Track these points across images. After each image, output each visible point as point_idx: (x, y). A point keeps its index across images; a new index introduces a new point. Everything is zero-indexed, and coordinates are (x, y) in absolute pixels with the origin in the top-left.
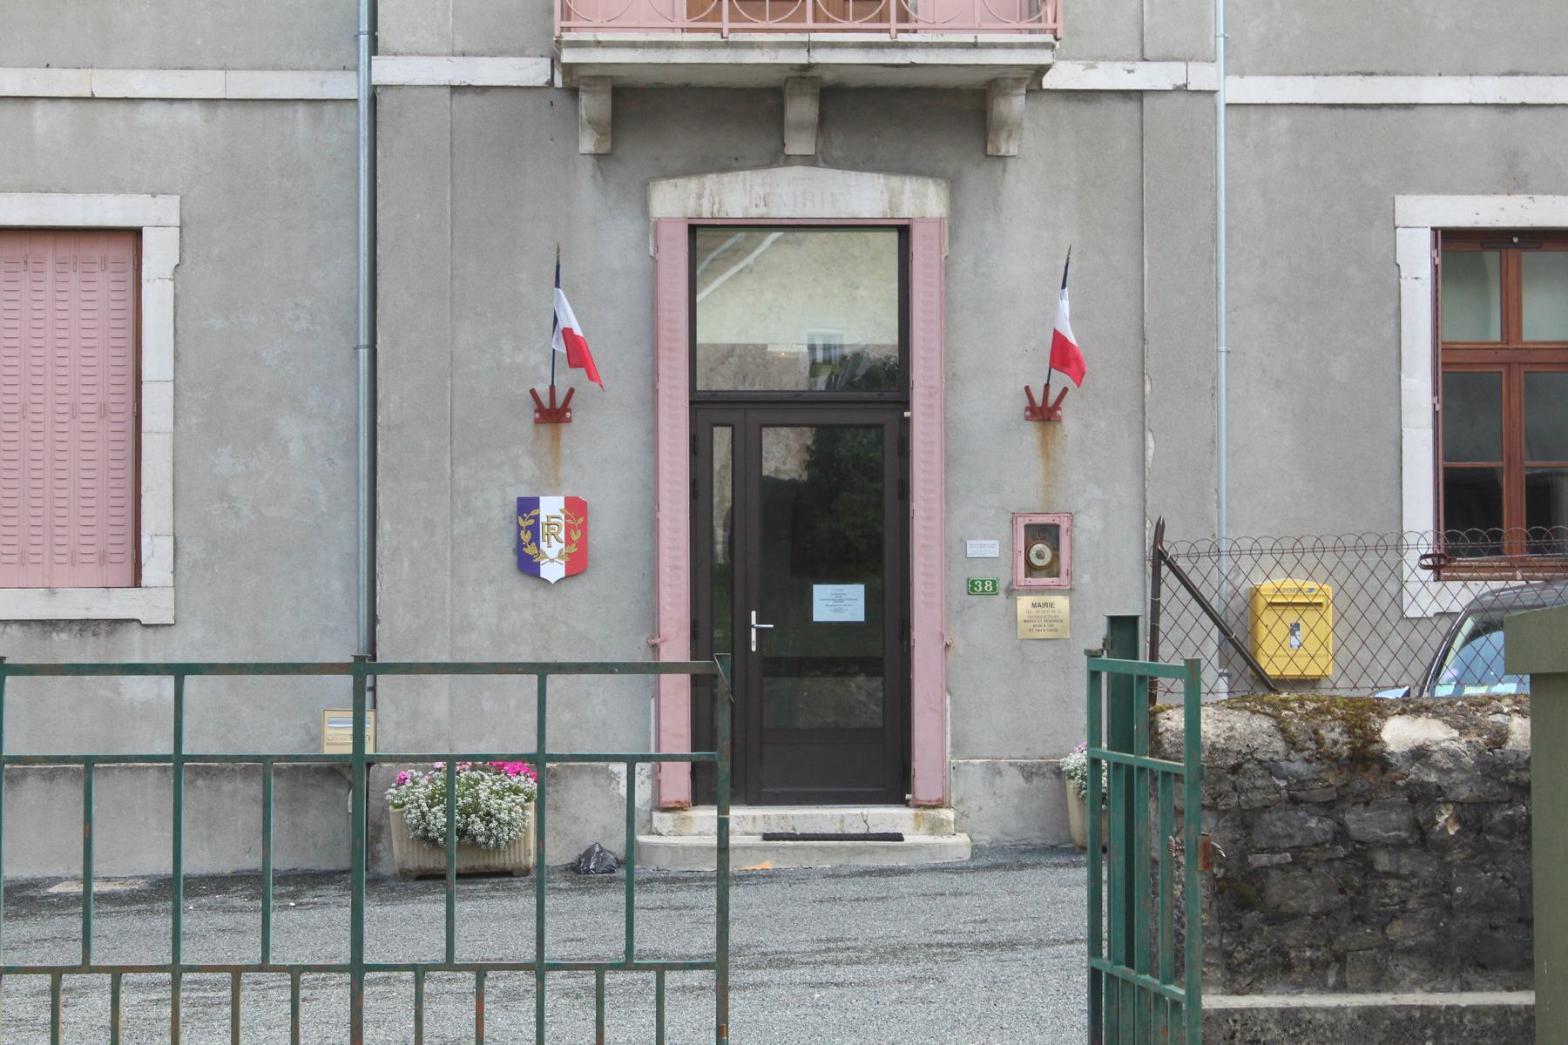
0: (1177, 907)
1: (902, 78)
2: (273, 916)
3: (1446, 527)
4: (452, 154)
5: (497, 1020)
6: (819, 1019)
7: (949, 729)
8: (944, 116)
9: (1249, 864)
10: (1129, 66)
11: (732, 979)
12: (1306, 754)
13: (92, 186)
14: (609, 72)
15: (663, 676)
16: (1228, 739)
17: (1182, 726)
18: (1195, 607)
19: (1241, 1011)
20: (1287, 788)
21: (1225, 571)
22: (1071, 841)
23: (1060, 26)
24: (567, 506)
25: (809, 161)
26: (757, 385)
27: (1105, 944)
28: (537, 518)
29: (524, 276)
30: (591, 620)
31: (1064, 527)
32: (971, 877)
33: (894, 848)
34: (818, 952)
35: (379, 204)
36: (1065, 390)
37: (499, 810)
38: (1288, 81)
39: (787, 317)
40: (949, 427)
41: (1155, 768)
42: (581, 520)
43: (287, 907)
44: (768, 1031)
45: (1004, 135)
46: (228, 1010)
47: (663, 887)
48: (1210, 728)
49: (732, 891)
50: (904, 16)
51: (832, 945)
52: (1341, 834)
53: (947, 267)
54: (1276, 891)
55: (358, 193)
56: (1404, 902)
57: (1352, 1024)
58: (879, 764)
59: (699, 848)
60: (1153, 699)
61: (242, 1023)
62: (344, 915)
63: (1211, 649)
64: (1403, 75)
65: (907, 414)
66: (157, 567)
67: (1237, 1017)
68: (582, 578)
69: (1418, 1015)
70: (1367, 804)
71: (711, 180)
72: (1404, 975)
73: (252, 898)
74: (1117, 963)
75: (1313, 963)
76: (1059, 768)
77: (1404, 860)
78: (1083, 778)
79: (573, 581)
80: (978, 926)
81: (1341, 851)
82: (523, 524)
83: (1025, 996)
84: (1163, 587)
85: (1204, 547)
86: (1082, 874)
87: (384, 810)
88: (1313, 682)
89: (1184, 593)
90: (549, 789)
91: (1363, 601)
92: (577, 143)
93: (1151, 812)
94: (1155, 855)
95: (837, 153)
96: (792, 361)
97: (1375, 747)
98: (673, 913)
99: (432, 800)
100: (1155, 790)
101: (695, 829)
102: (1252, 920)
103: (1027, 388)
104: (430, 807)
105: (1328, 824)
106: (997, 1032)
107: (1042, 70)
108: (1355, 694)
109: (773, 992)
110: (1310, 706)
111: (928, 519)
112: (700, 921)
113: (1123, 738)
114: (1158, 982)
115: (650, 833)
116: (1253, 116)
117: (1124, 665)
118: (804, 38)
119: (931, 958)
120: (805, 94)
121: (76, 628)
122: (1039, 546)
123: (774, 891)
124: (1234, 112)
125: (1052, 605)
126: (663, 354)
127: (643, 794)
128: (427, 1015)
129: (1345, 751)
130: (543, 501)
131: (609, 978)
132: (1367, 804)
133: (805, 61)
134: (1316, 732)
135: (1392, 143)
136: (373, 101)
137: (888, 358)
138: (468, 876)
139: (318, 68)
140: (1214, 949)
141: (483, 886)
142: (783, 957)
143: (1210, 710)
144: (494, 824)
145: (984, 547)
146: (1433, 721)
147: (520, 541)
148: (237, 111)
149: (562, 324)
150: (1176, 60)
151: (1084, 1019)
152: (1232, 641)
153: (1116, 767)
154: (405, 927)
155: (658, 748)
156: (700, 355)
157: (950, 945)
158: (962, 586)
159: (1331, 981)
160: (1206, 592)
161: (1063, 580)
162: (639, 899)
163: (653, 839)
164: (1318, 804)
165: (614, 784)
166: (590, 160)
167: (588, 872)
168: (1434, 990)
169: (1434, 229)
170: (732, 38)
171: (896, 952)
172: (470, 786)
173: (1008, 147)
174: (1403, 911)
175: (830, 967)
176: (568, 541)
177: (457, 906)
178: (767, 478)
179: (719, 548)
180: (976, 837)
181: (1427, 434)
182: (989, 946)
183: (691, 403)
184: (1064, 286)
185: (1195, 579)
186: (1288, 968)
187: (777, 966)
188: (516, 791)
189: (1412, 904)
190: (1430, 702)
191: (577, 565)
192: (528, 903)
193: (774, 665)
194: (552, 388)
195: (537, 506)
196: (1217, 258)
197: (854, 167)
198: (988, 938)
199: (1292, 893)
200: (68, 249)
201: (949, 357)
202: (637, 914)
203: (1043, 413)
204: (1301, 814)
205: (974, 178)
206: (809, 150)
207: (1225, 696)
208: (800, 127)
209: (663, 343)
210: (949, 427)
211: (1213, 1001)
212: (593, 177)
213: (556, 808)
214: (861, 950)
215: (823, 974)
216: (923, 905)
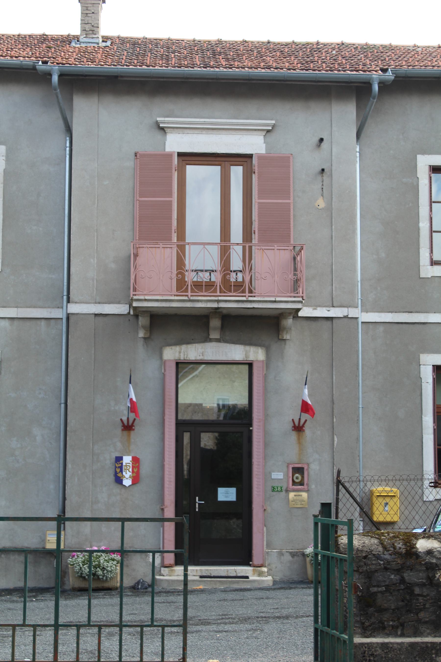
0: (345, 606)
1: (250, 312)
2: (27, 604)
3: (438, 473)
4: (95, 337)
5: (105, 643)
6: (219, 644)
7: (265, 539)
8: (265, 326)
9: (370, 591)
10: (328, 309)
11: (188, 629)
12: (390, 552)
14: (149, 310)
15: (165, 523)
16: (363, 546)
17: (347, 542)
18: (351, 500)
19: (368, 644)
20: (384, 564)
21: (362, 487)
22: (308, 579)
23: (304, 295)
26: (198, 417)
27: (320, 617)
28: (122, 464)
29: (119, 379)
30: (140, 502)
32: (272, 592)
34: (219, 619)
35: (69, 354)
37: (107, 567)
38: (383, 315)
39: (208, 394)
40: (266, 433)
41: (337, 557)
42: (137, 464)
43: (32, 601)
44: (201, 649)
45: (285, 332)
46: (11, 639)
47: (165, 594)
48: (356, 543)
49: (189, 596)
50: (251, 291)
51: (224, 617)
52: (402, 581)
53: (265, 377)
54: (380, 600)
55: (62, 350)
56: (424, 605)
57: (406, 648)
59: (178, 581)
60: (336, 532)
61: (16, 644)
62: (52, 604)
63: (357, 514)
64: (422, 313)
65: (251, 428)
67: (366, 646)
68: (137, 485)
69: (429, 645)
70: (411, 570)
71: (184, 347)
72: (424, 631)
73: (20, 597)
74: (324, 626)
75: (393, 626)
76: (304, 553)
77: (425, 590)
78: (312, 557)
79: (134, 486)
80: (275, 610)
81: (402, 587)
82: (117, 466)
83: (291, 636)
84: (340, 493)
86: (312, 591)
87: (67, 566)
88: (391, 523)
89: (347, 495)
90: (125, 559)
91: (410, 498)
92: (138, 333)
93: (336, 572)
94: (338, 587)
96: (211, 409)
97: (414, 550)
98: (168, 604)
99: (84, 563)
100: (337, 564)
101: (176, 574)
102: (372, 612)
103: (293, 420)
104: (83, 565)
105: (398, 577)
106: (282, 649)
107: (298, 310)
108: (407, 531)
109: (202, 634)
110: (392, 535)
111: (258, 465)
112: (177, 607)
113: (326, 547)
114: (338, 633)
115: (160, 575)
116: (371, 326)
117: (326, 520)
118: (216, 298)
119: (258, 622)
122: (297, 475)
123: (204, 596)
124: (364, 325)
127: (158, 561)
128: (81, 641)
129: (404, 551)
131: (145, 629)
132: (411, 570)
133: (216, 306)
134: (393, 544)
136: (68, 319)
137: (245, 407)
138: (97, 590)
139: (49, 307)
140: (358, 621)
141: (101, 594)
142: (206, 621)
143: (357, 536)
144: (105, 572)
145: (278, 475)
146: (434, 541)
147: (116, 472)
149: (130, 397)
150: (344, 307)
151: (312, 645)
152: (364, 512)
153: (323, 556)
154: (74, 609)
155: (163, 548)
156: (179, 406)
157: (265, 617)
158: (270, 489)
159: (399, 633)
160: (355, 495)
161: (305, 487)
162: (156, 599)
163: (161, 577)
164: (394, 570)
165: (148, 558)
166: (142, 340)
167: (138, 589)
168: (435, 636)
169: (433, 366)
170: (192, 298)
171: (246, 620)
172: (97, 558)
173: (287, 336)
174: (424, 608)
175: (223, 625)
176: (133, 472)
177: (92, 601)
178: (202, 448)
179: (185, 472)
180: (275, 577)
181: (432, 437)
182: (279, 617)
183: (177, 424)
184: (306, 384)
185: (351, 490)
186: (384, 628)
187: (204, 625)
188: (113, 560)
189: (427, 606)
190: (433, 534)
191: (136, 480)
192: (117, 600)
194: (128, 419)
196: (359, 375)
198: (278, 615)
199: (385, 601)
201: (266, 408)
202: (155, 604)
203: (298, 428)
204: (388, 573)
206: (218, 337)
207: (362, 531)
208: (215, 329)
210: (266, 433)
211: (358, 640)
212: (143, 345)
213: (127, 566)
214: (234, 619)
215: (221, 628)
216: (255, 602)
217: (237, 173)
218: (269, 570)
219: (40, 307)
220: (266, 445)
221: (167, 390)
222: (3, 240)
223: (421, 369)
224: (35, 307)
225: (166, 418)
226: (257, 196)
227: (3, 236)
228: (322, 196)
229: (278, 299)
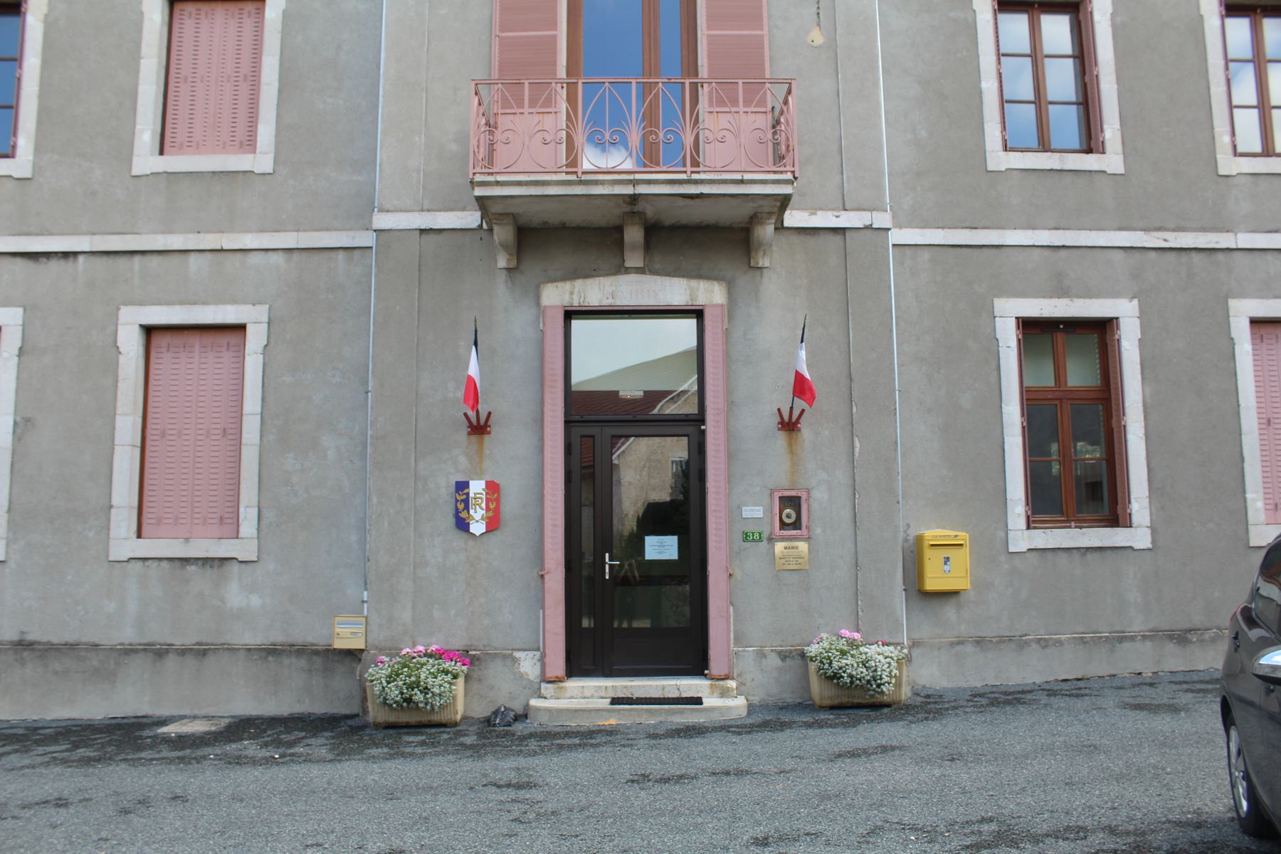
13: (220, 300)
22: (811, 699)
23: (797, 169)
25: (640, 271)
28: (468, 494)
31: (804, 498)
33: (697, 710)
36: (803, 411)
38: (928, 232)
39: (610, 355)
45: (761, 254)
66: (248, 527)
71: (579, 283)
79: (490, 535)
101: (568, 695)
104: (388, 683)
111: (717, 493)
115: (541, 697)
116: (908, 251)
121: (200, 563)
122: (788, 511)
124: (897, 249)
135: (983, 270)
148: (304, 255)
150: (864, 210)
158: (738, 536)
161: (804, 531)
166: (505, 272)
173: (764, 262)
176: (488, 509)
181: (1019, 440)
188: (446, 672)
191: (493, 524)
193: (622, 580)
197: (668, 274)
200: (208, 339)
201: (729, 391)
203: (789, 426)
205: (743, 280)
208: (633, 248)
209: (548, 383)
218: (741, 684)
219: (336, 230)
220: (731, 456)
221: (548, 359)
222: (277, 123)
223: (998, 324)
224: (327, 230)
225: (547, 408)
226: (705, 26)
227: (278, 116)
228: (819, 25)
229: (747, 177)
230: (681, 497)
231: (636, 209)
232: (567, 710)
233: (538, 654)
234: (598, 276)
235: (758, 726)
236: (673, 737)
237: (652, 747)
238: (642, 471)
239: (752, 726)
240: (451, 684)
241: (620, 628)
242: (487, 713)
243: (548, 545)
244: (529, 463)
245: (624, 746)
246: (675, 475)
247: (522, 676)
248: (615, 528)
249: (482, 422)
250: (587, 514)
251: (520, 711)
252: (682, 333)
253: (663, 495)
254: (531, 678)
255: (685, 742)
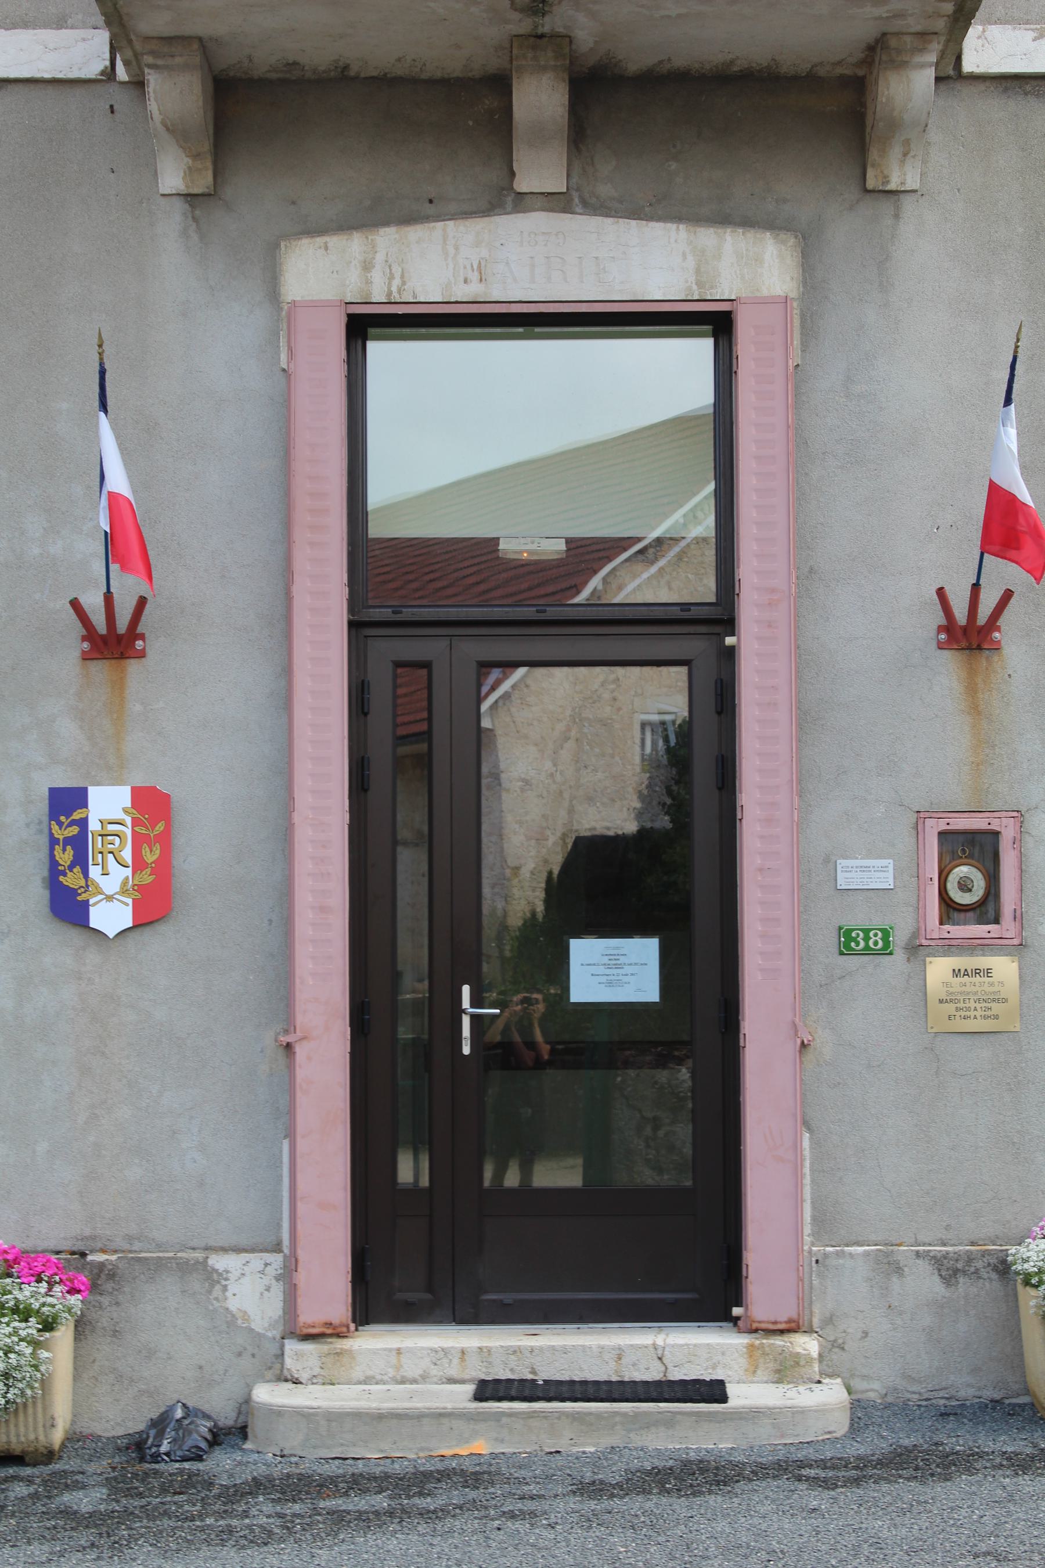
22: (1027, 1391)
24: (134, 804)
25: (556, 202)
28: (83, 823)
31: (1008, 832)
36: (1008, 595)
39: (467, 438)
40: (802, 661)
42: (160, 827)
45: (896, 151)
53: (798, 379)
58: (685, 1251)
65: (729, 641)
68: (162, 928)
71: (386, 238)
76: (1004, 1262)
79: (146, 934)
82: (59, 834)
85: (394, 1360)
95: (605, 190)
101: (358, 1373)
103: (941, 592)
120: (544, 69)
122: (963, 870)
125: (988, 972)
126: (301, 536)
130: (93, 792)
147: (53, 863)
161: (1007, 927)
165: (217, 1290)
166: (179, 205)
173: (903, 175)
176: (138, 864)
180: (858, 1384)
184: (1008, 401)
188: (23, 1313)
191: (153, 906)
193: (501, 1054)
194: (108, 597)
195: (84, 803)
197: (636, 213)
203: (969, 635)
209: (302, 517)
210: (802, 661)
212: (184, 233)
217: (424, 727)
220: (805, 720)
230: (664, 822)
231: (547, 25)
232: (357, 1415)
233: (276, 1260)
234: (439, 218)
235: (880, 1463)
236: (645, 1492)
237: (588, 1521)
238: (560, 756)
239: (863, 1463)
240: (36, 1344)
241: (499, 1192)
242: (137, 1425)
243: (305, 964)
244: (251, 747)
245: (512, 1516)
246: (650, 763)
247: (232, 1321)
248: (486, 910)
249: (984, 614)
250: (410, 868)
251: (227, 1417)
252: (676, 374)
253: (618, 817)
254: (259, 1324)
255: (680, 1505)
